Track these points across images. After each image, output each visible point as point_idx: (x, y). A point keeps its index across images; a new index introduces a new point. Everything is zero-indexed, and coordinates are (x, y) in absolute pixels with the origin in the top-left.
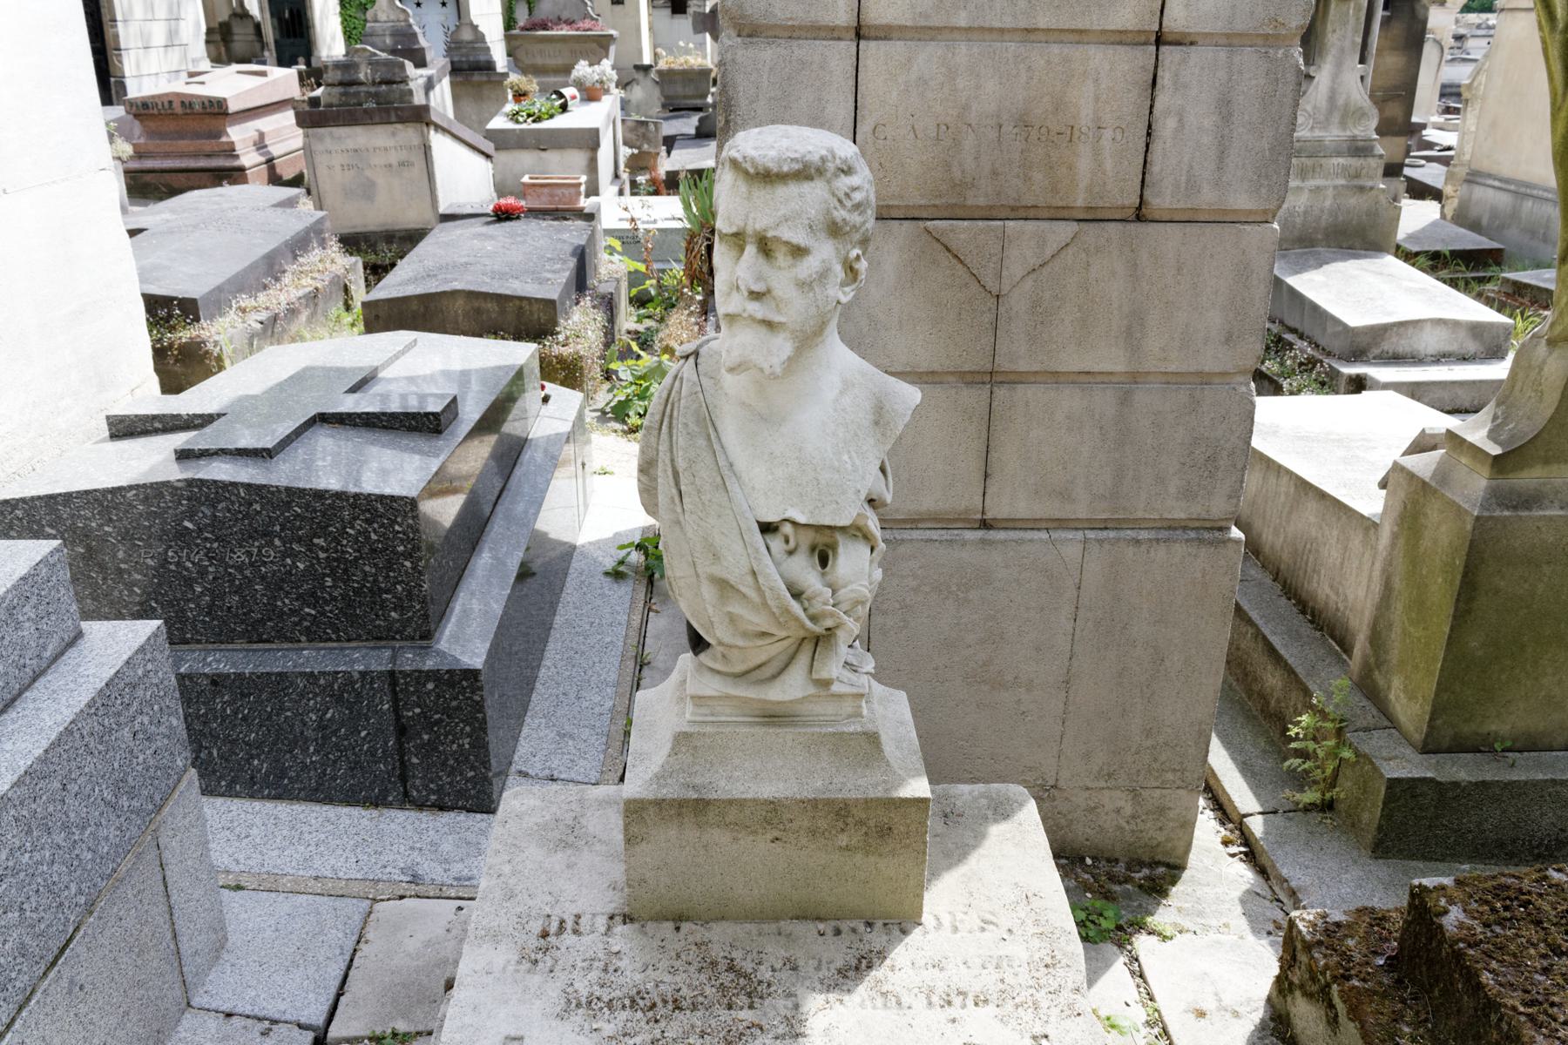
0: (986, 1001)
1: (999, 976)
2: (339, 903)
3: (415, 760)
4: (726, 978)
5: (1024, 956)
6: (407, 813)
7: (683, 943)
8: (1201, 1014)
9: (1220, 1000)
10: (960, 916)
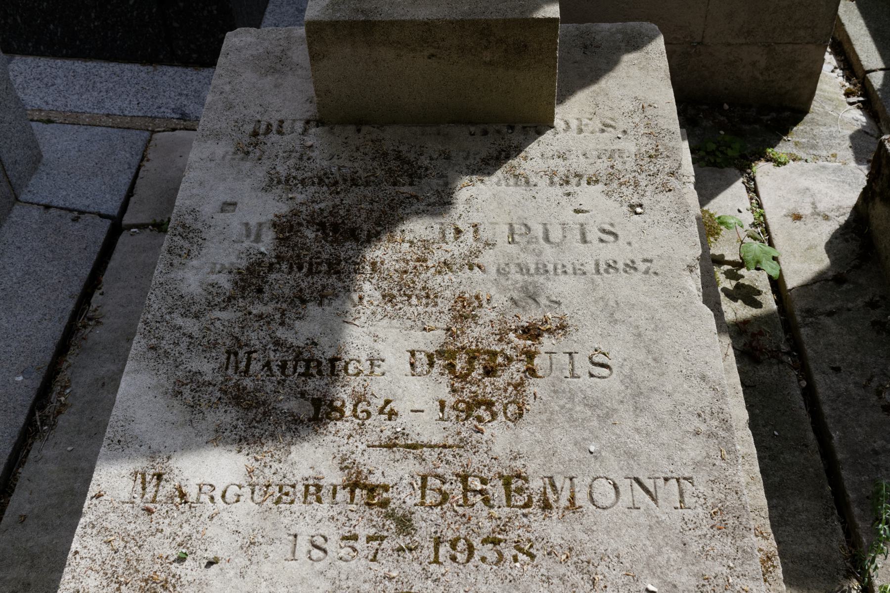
0: (597, 181)
1: (610, 164)
2: (126, 133)
3: (176, 25)
4: (393, 164)
5: (633, 149)
6: (176, 68)
7: (362, 140)
8: (797, 217)
9: (816, 208)
10: (585, 121)
